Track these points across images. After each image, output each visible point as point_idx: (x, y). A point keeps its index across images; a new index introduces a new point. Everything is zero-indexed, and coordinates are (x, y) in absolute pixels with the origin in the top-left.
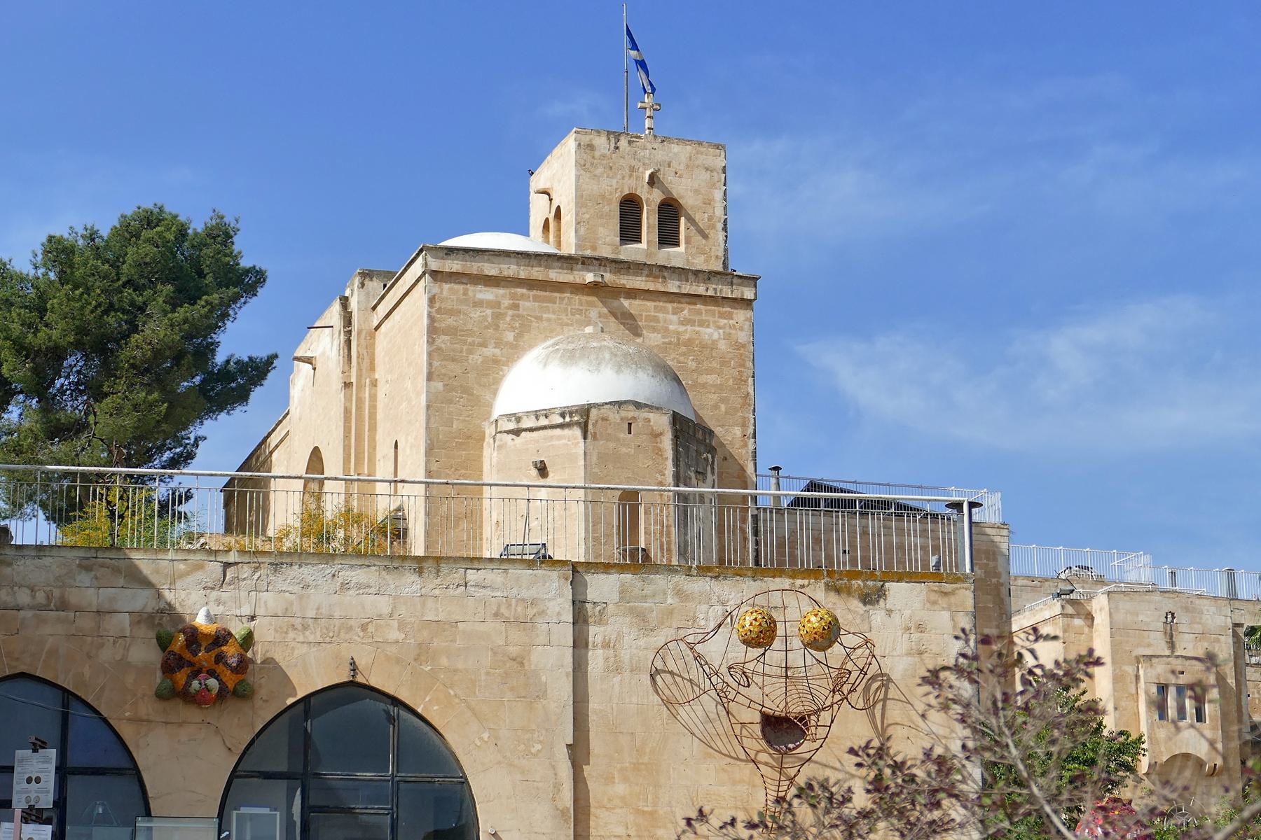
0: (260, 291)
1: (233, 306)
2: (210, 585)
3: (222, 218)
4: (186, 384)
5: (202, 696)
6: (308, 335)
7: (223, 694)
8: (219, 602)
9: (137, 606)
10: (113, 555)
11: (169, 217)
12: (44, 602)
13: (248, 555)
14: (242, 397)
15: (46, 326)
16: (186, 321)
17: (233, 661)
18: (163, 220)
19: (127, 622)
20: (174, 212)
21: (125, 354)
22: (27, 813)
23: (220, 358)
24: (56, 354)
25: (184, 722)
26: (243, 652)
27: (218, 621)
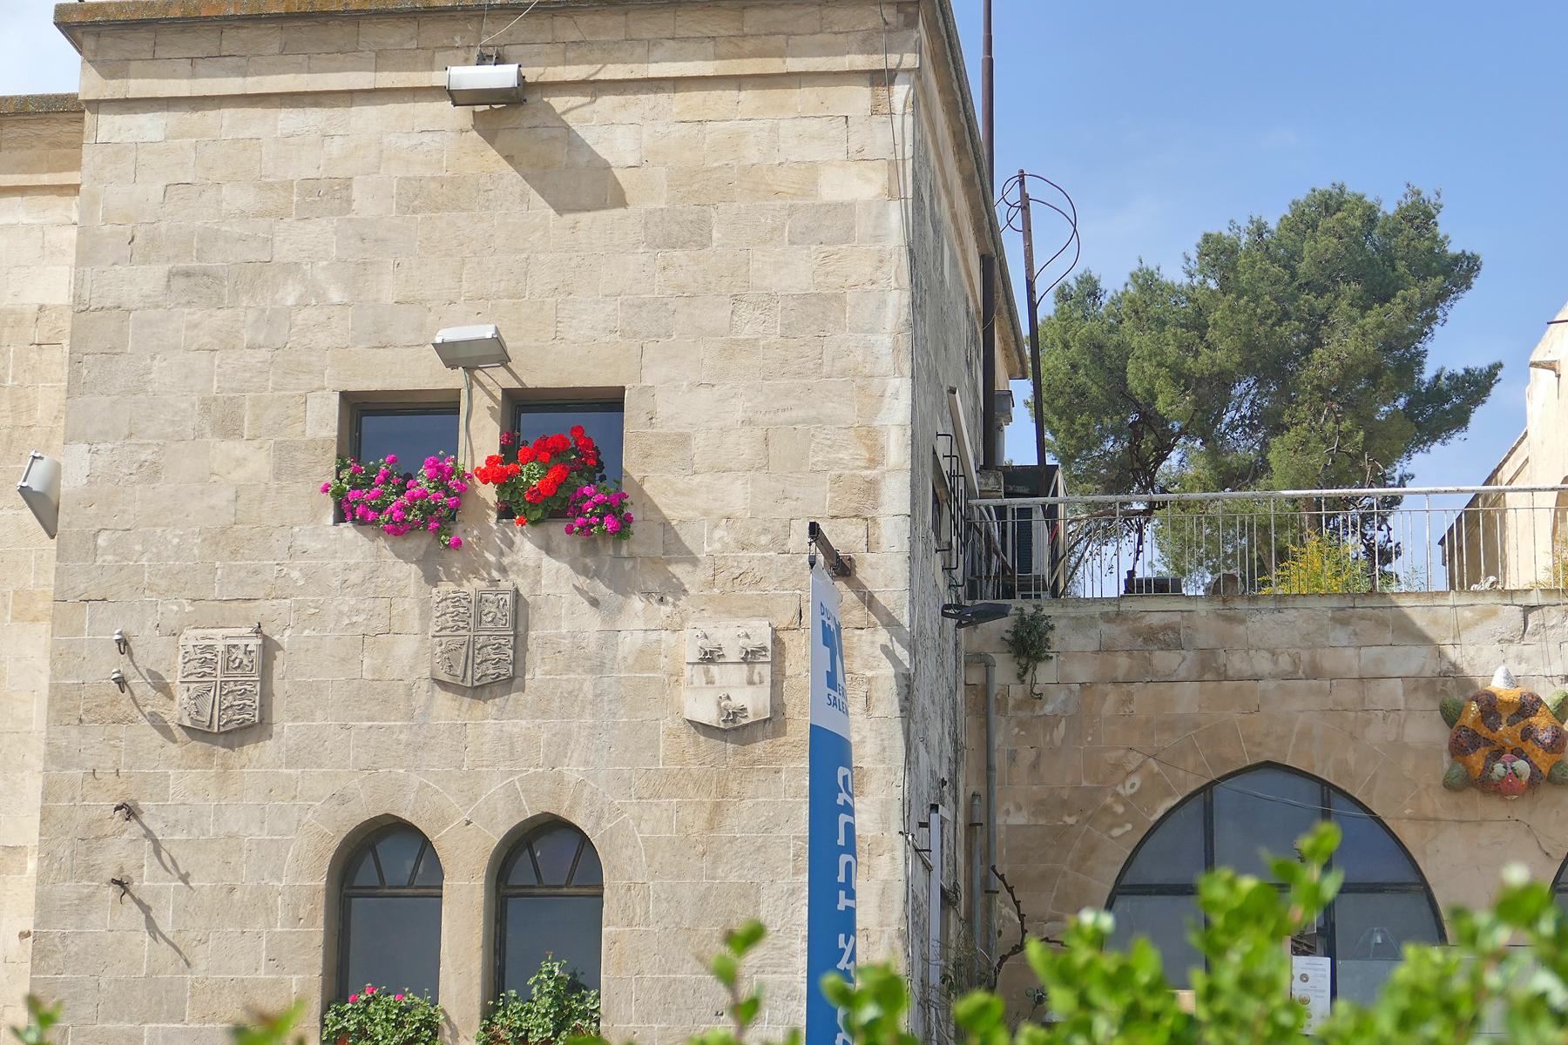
0: (1476, 282)
1: (1441, 305)
2: (1506, 636)
3: (1419, 194)
4: (1386, 408)
5: (1509, 783)
6: (1548, 333)
7: (1535, 781)
8: (1520, 659)
9: (1412, 667)
10: (1375, 602)
11: (1354, 199)
12: (1289, 668)
13: (1556, 594)
14: (1460, 420)
15: (1208, 347)
16: (1380, 325)
17: (1546, 736)
18: (1345, 202)
19: (1400, 691)
20: (1359, 192)
21: (1306, 374)
22: (1297, 942)
23: (1428, 375)
24: (1222, 382)
25: (1484, 820)
26: (1558, 724)
27: (1521, 683)
